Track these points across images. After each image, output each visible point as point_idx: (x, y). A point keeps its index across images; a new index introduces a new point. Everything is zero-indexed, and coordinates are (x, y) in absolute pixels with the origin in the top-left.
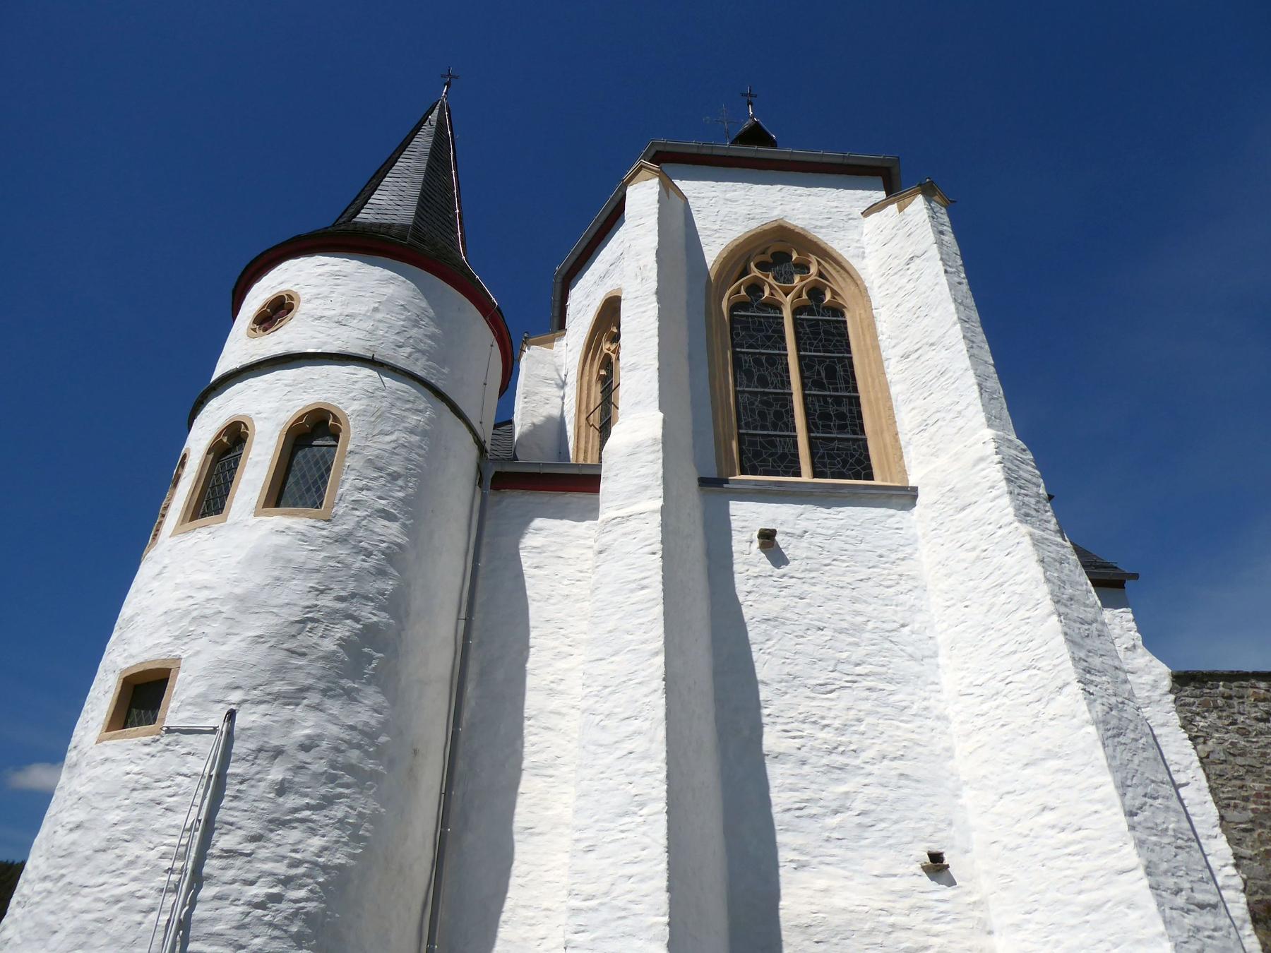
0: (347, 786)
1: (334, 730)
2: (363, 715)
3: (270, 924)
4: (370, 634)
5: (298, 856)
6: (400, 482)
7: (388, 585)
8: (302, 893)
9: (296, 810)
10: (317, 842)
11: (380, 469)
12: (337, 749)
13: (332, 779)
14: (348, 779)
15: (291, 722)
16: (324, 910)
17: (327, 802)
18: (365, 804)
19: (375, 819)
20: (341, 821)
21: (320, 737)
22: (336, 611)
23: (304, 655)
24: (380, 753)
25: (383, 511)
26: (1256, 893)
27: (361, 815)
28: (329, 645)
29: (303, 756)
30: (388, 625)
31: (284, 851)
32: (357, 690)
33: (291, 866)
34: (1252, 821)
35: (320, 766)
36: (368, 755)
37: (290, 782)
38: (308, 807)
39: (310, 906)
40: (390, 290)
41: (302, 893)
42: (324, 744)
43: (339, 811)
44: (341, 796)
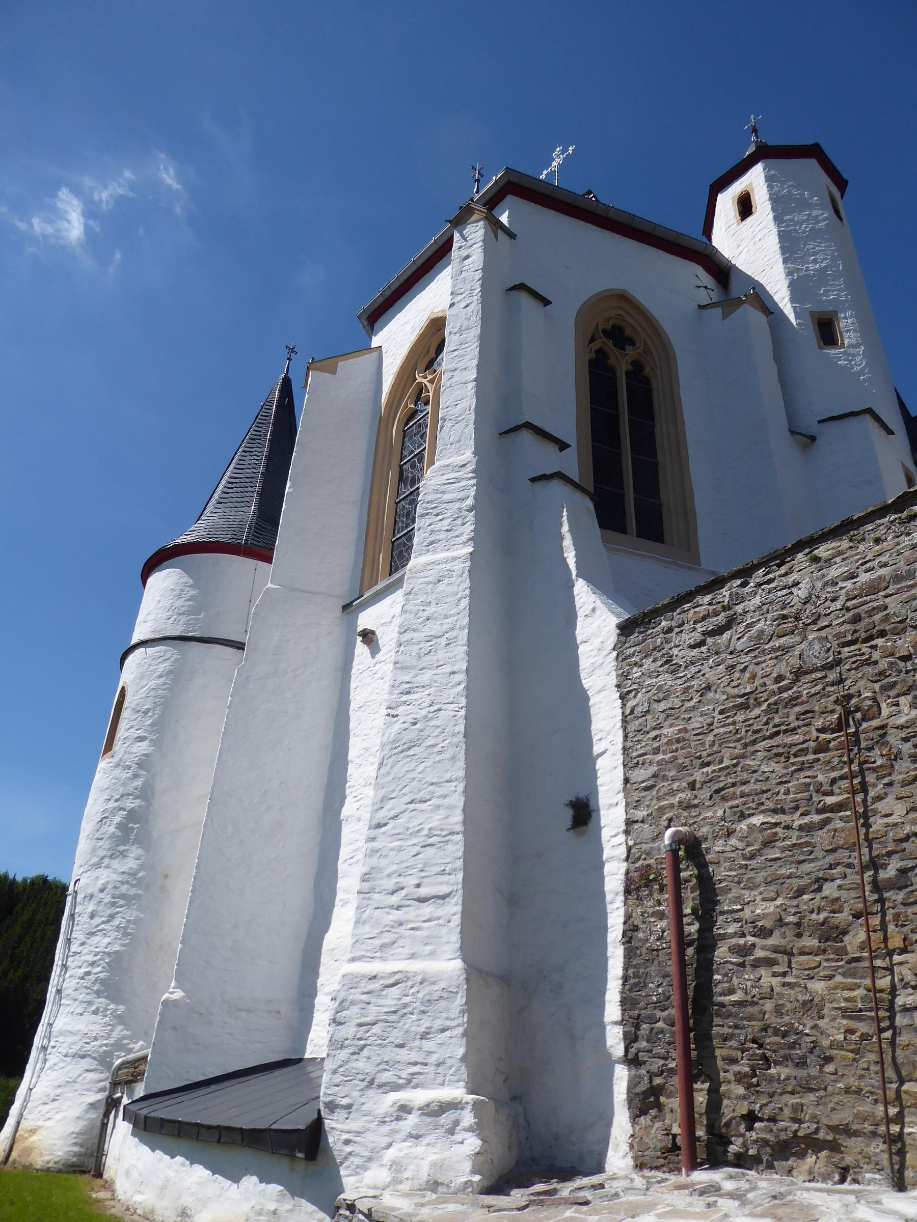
0: (121, 906)
1: (115, 877)
2: (130, 864)
3: (86, 987)
4: (132, 816)
5: (97, 950)
6: (150, 714)
7: (139, 783)
8: (99, 969)
9: (98, 925)
10: (107, 940)
11: (138, 712)
12: (116, 888)
13: (113, 904)
14: (122, 902)
15: (97, 878)
16: (111, 975)
17: (112, 917)
18: (132, 914)
19: (137, 921)
20: (117, 927)
21: (108, 883)
22: (115, 809)
23: (102, 839)
24: (139, 883)
25: (138, 737)
26: (639, 859)
27: (128, 921)
28: (112, 829)
29: (101, 895)
30: (140, 807)
31: (92, 949)
32: (127, 850)
33: (95, 955)
34: (654, 776)
35: (108, 899)
36: (133, 886)
37: (96, 911)
38: (104, 923)
39: (102, 975)
40: (185, 580)
41: (99, 969)
42: (110, 886)
43: (116, 922)
44: (118, 913)
